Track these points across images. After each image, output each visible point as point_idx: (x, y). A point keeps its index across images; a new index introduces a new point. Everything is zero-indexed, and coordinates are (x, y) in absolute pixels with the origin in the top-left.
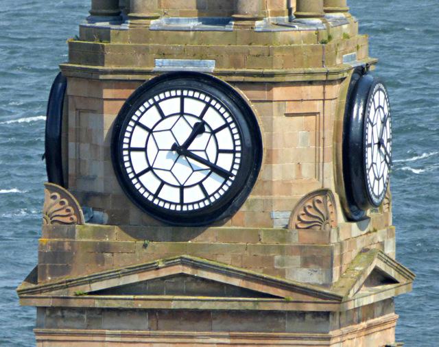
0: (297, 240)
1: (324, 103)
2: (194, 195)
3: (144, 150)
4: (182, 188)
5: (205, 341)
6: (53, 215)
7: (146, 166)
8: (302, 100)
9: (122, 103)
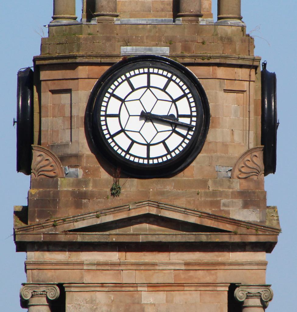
0: (239, 187)
1: (249, 83)
2: (158, 151)
3: (118, 116)
4: (148, 145)
5: (164, 268)
6: (39, 170)
7: (177, 103)
8: (235, 80)
9: (95, 82)
